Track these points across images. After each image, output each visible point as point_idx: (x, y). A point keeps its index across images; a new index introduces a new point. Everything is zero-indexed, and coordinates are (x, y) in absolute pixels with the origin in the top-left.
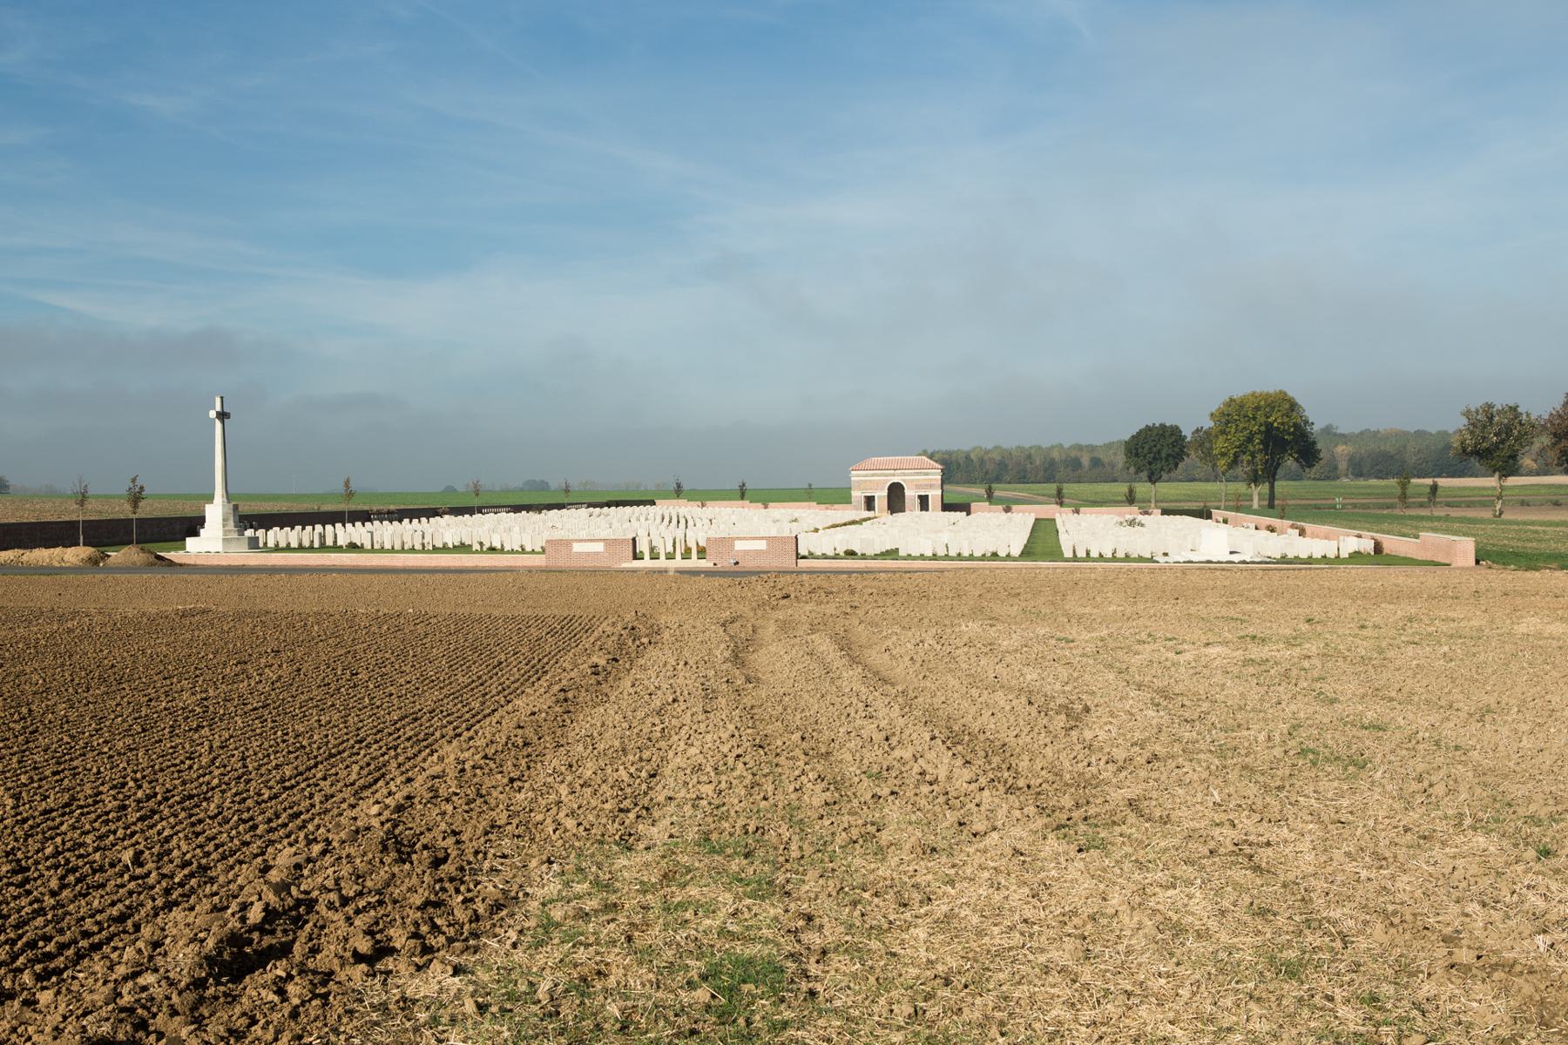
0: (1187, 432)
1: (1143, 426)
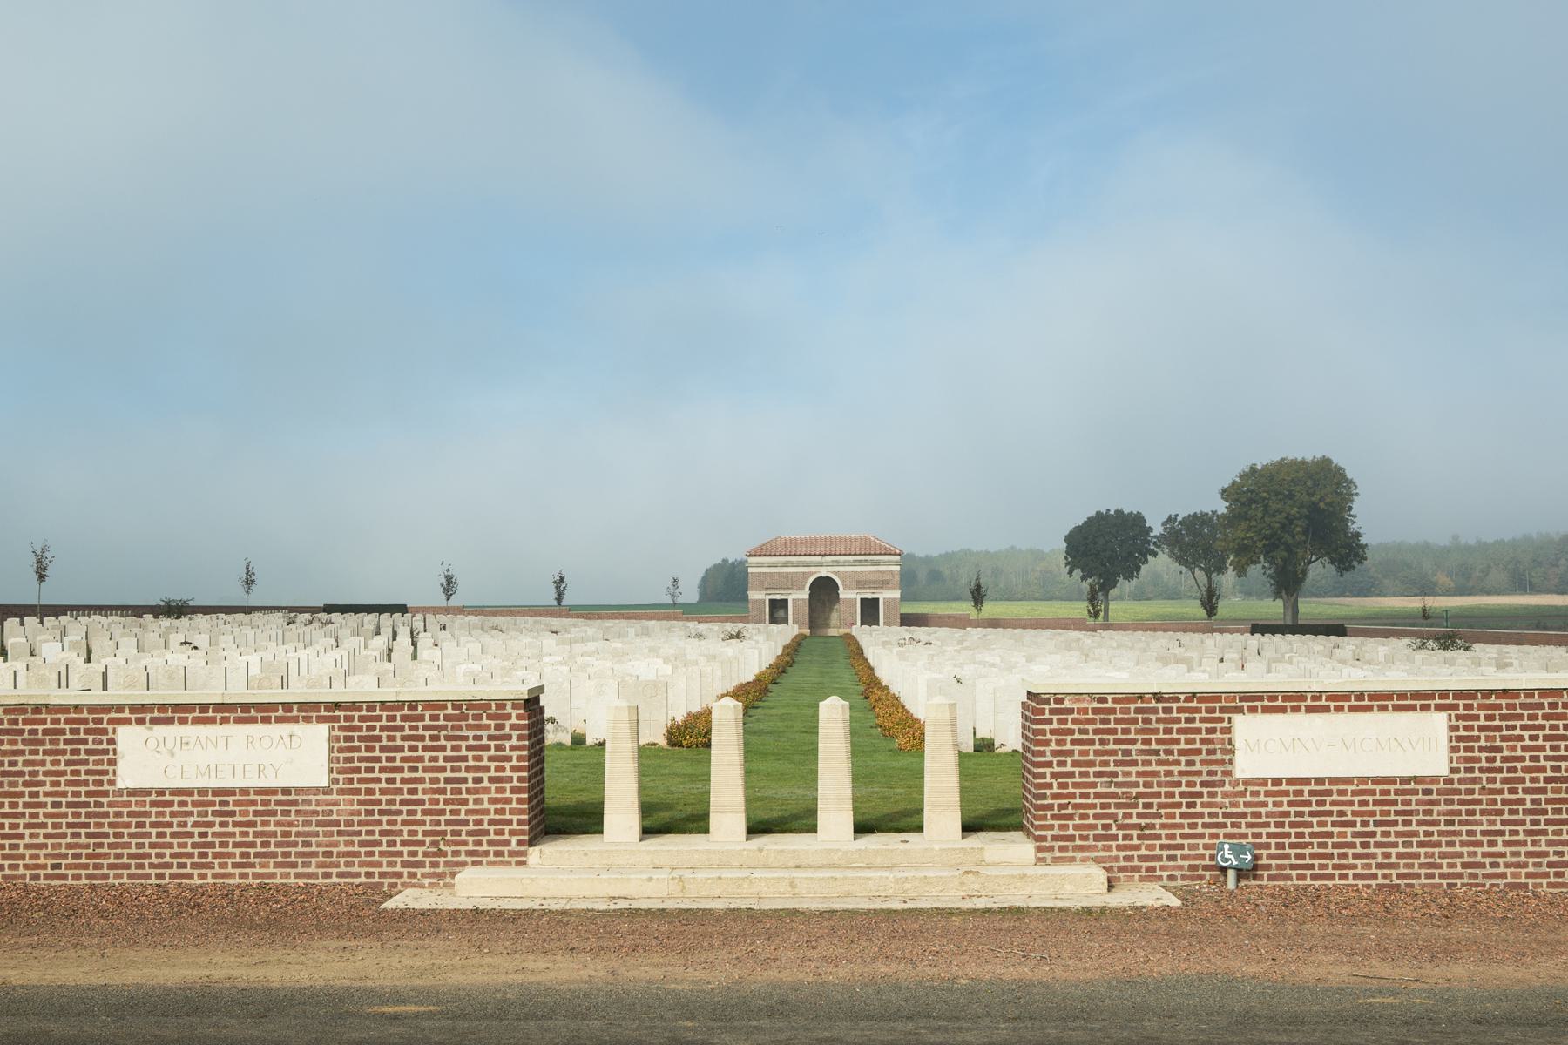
1: (1093, 513)
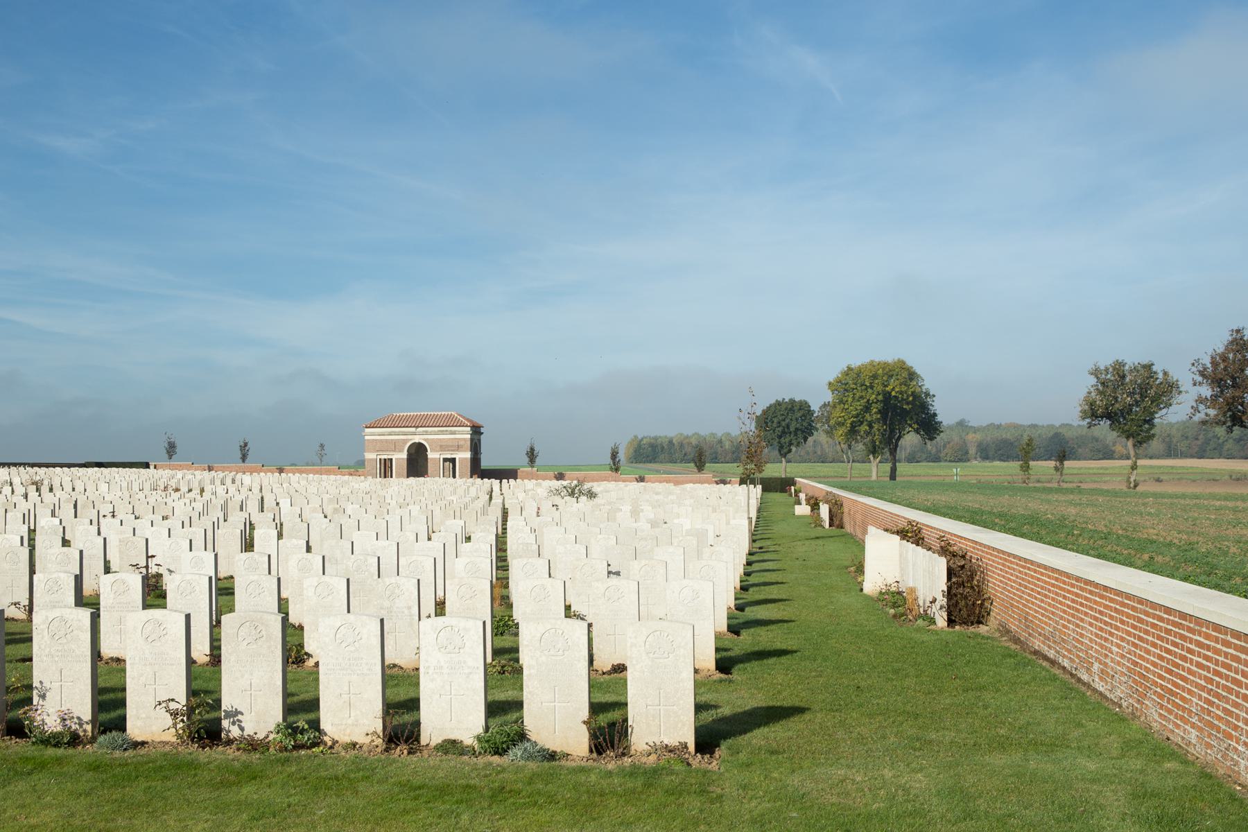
0: (815, 406)
1: (773, 401)
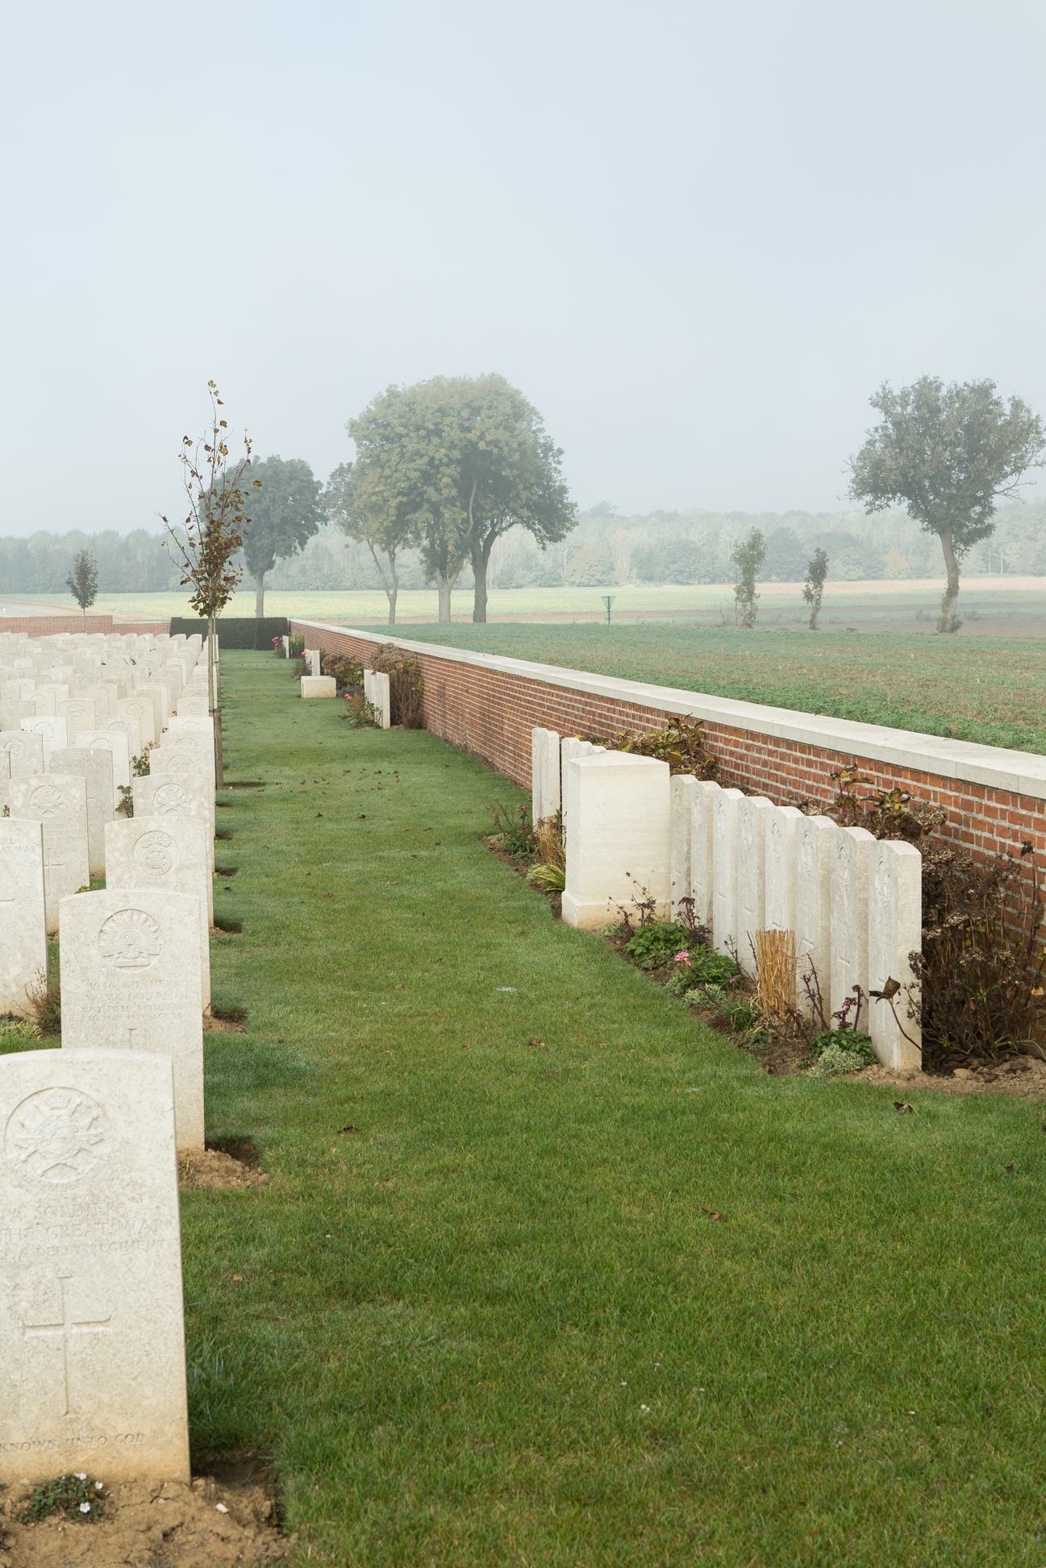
0: (322, 474)
